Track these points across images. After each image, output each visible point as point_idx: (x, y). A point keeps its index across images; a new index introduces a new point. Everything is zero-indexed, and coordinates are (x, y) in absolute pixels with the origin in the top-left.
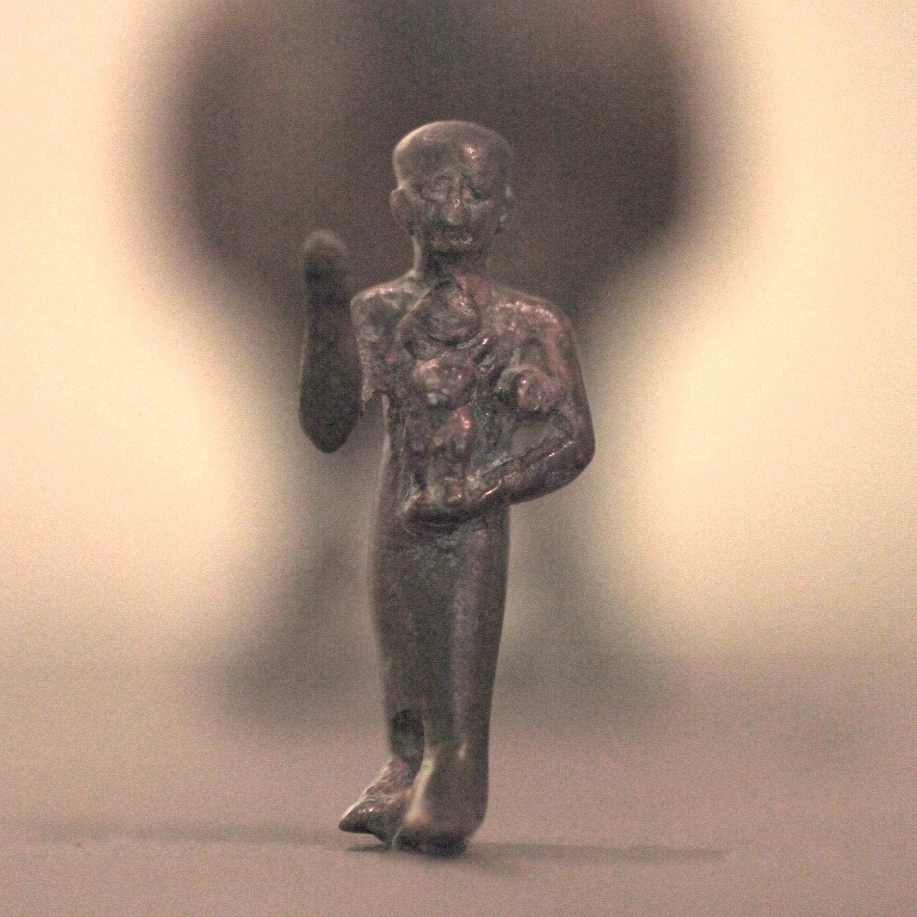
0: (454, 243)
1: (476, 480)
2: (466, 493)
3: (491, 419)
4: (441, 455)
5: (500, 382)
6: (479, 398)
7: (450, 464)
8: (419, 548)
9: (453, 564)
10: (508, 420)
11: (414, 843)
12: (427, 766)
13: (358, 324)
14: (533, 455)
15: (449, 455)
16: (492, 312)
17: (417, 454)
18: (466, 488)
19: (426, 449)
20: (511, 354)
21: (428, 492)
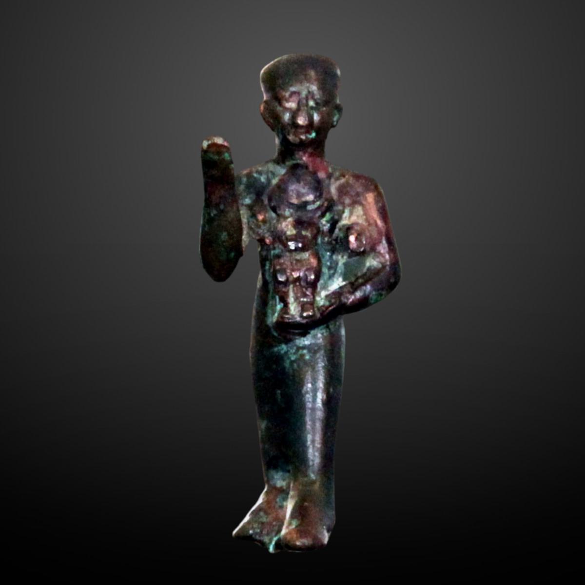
0: (303, 137)
1: (322, 299)
2: (316, 309)
3: (331, 257)
4: (298, 284)
5: (337, 230)
6: (323, 243)
7: (304, 289)
8: (279, 480)
9: (307, 357)
10: (343, 257)
11: (276, 290)
12: (243, 214)
13: (239, 192)
14: (360, 281)
15: (303, 283)
16: (292, 362)
17: (281, 282)
18: (315, 305)
19: (287, 280)
20: (343, 212)
21: (289, 309)
